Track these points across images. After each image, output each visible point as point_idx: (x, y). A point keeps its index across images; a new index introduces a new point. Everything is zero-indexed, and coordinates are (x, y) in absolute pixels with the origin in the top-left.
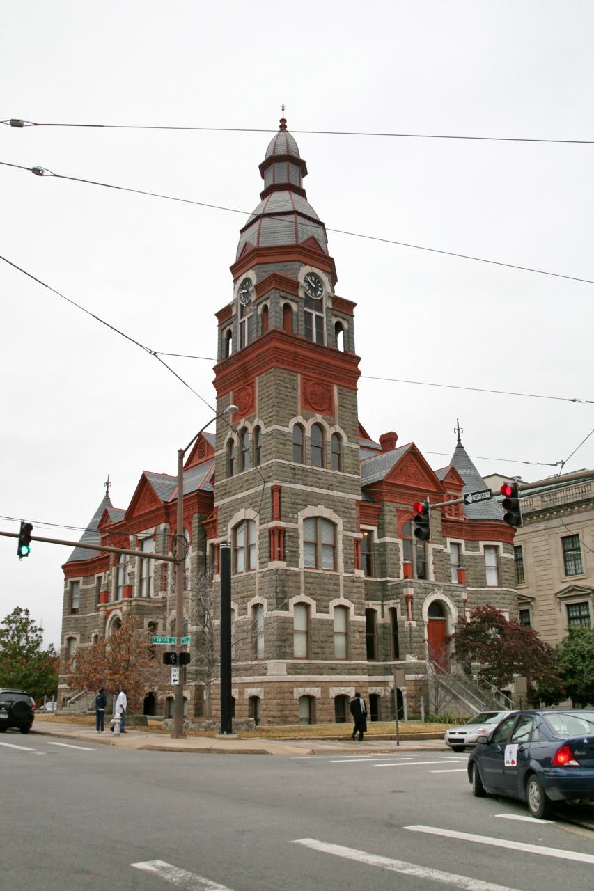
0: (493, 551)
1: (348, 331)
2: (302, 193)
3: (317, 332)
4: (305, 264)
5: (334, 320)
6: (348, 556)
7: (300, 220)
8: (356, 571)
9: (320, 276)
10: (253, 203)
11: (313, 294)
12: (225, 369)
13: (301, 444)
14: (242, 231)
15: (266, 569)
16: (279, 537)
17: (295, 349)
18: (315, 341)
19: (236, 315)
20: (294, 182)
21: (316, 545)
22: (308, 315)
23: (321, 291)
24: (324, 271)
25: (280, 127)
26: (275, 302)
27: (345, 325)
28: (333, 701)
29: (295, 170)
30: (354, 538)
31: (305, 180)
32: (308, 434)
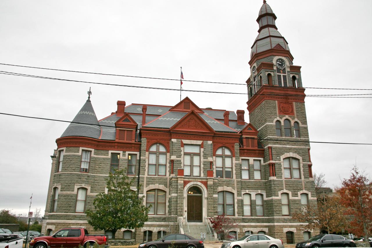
0: (258, 162)
1: (299, 79)
2: (274, 27)
3: (284, 82)
4: (276, 56)
5: (291, 76)
6: (279, 171)
7: (272, 38)
8: (310, 178)
9: (283, 59)
10: (255, 35)
11: (281, 67)
12: (250, 103)
13: (290, 128)
14: (252, 48)
15: (308, 180)
16: (272, 167)
17: (284, 92)
18: (283, 86)
19: (252, 81)
20: (271, 23)
21: (290, 169)
22: (279, 76)
23: (284, 65)
24: (285, 57)
25: (264, 2)
26: (264, 74)
27: (297, 77)
28: (285, 234)
29: (270, 18)
30: (308, 164)
31: (276, 21)
32: (282, 124)
